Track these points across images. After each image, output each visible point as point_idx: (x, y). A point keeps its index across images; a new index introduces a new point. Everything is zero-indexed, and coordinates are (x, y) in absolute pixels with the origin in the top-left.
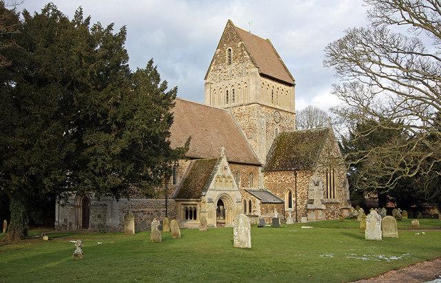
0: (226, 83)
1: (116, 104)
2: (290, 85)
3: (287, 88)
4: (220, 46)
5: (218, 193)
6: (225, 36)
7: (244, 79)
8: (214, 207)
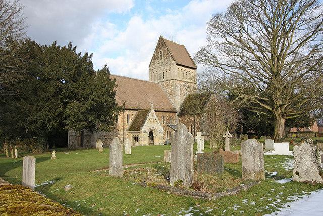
0: (160, 69)
1: (84, 89)
2: (194, 69)
3: (193, 70)
4: (156, 50)
5: (150, 128)
6: (159, 44)
7: (169, 67)
8: (147, 135)
